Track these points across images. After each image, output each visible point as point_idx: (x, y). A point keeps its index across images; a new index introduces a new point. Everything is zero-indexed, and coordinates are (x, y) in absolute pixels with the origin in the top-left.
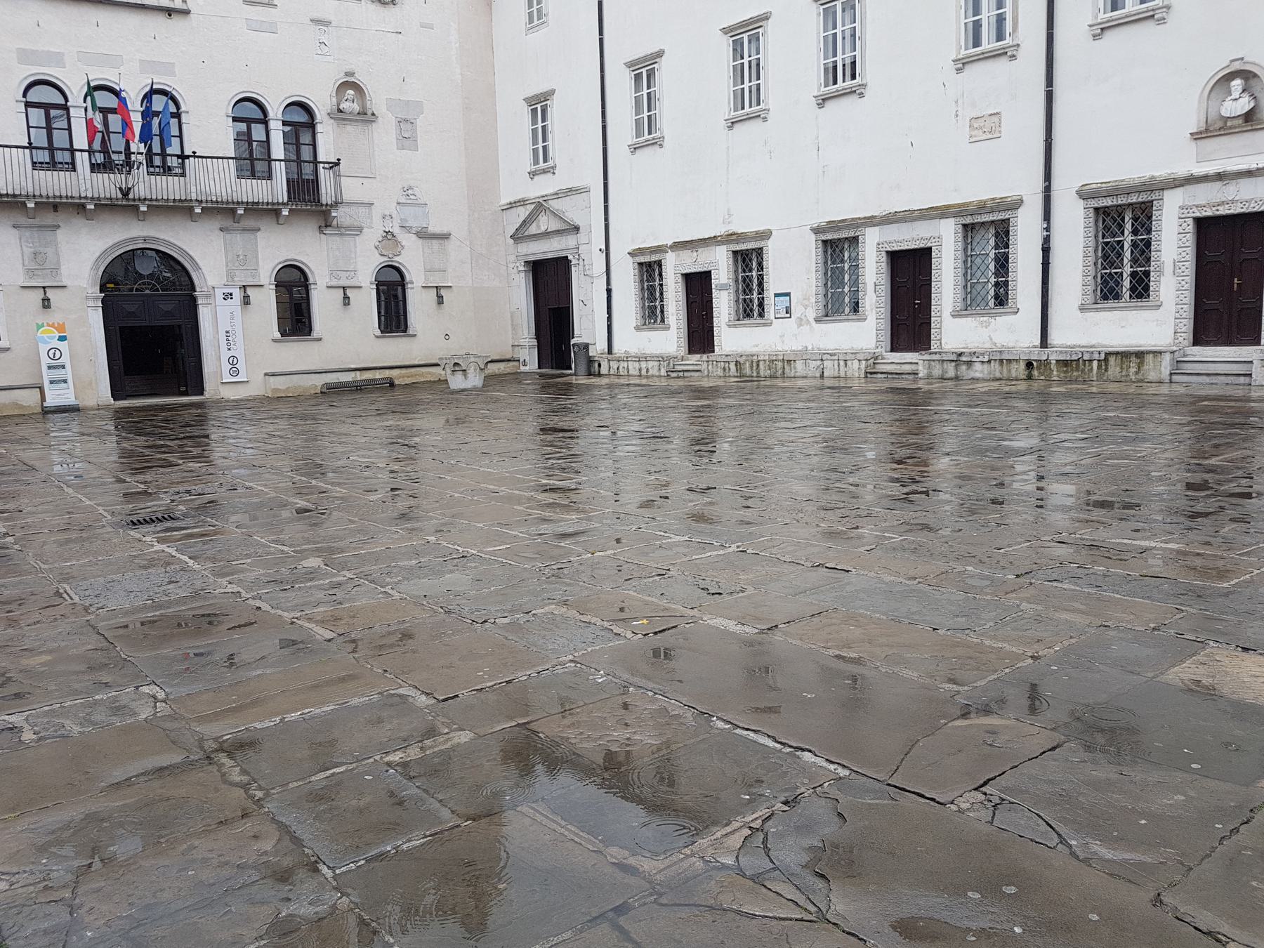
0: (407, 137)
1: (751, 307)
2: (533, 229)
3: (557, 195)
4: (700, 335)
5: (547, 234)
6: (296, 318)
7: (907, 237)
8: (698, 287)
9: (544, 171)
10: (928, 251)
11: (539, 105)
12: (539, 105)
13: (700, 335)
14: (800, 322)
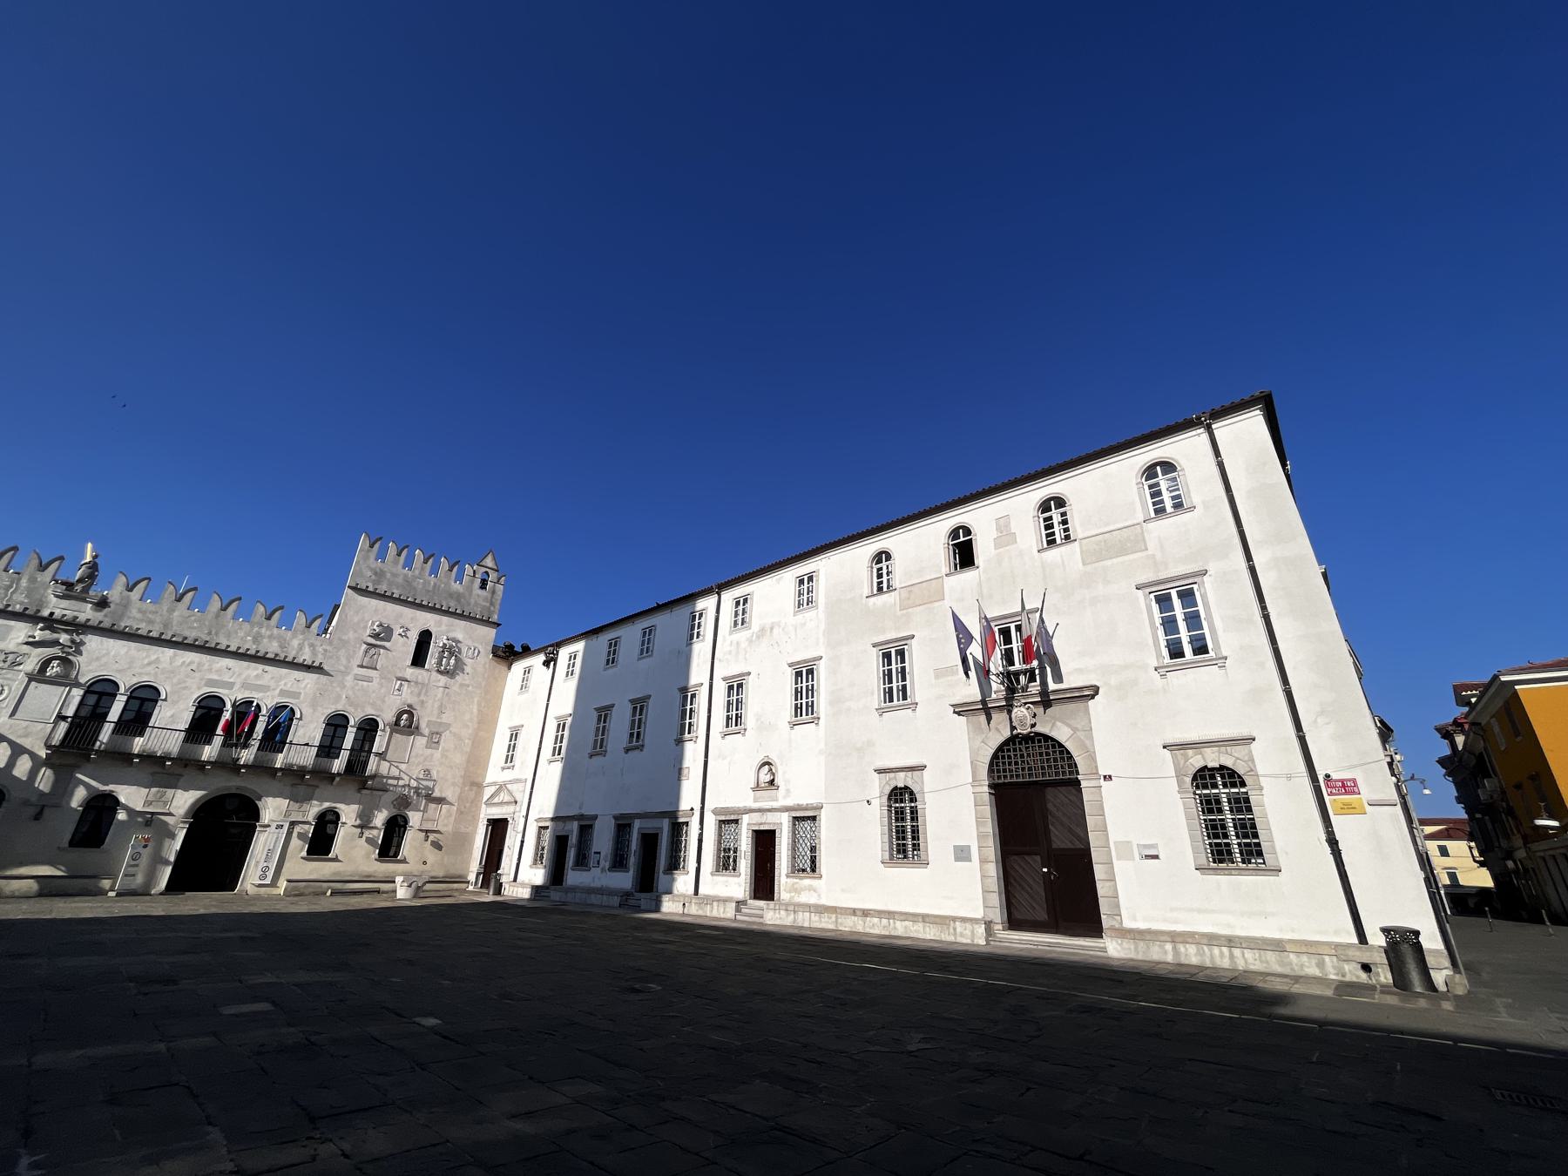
0: (434, 740)
1: (582, 862)
2: (496, 800)
3: (511, 782)
4: (763, 885)
5: (502, 804)
6: (320, 844)
7: (650, 825)
8: (765, 841)
9: (636, 748)
10: (773, 832)
11: (514, 736)
12: (514, 736)
13: (763, 885)
14: (603, 870)
